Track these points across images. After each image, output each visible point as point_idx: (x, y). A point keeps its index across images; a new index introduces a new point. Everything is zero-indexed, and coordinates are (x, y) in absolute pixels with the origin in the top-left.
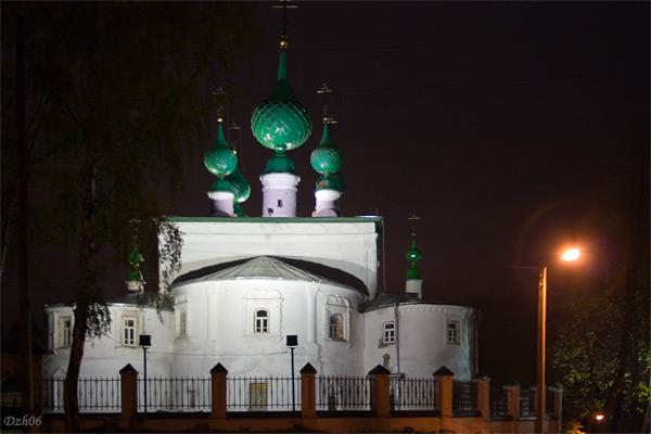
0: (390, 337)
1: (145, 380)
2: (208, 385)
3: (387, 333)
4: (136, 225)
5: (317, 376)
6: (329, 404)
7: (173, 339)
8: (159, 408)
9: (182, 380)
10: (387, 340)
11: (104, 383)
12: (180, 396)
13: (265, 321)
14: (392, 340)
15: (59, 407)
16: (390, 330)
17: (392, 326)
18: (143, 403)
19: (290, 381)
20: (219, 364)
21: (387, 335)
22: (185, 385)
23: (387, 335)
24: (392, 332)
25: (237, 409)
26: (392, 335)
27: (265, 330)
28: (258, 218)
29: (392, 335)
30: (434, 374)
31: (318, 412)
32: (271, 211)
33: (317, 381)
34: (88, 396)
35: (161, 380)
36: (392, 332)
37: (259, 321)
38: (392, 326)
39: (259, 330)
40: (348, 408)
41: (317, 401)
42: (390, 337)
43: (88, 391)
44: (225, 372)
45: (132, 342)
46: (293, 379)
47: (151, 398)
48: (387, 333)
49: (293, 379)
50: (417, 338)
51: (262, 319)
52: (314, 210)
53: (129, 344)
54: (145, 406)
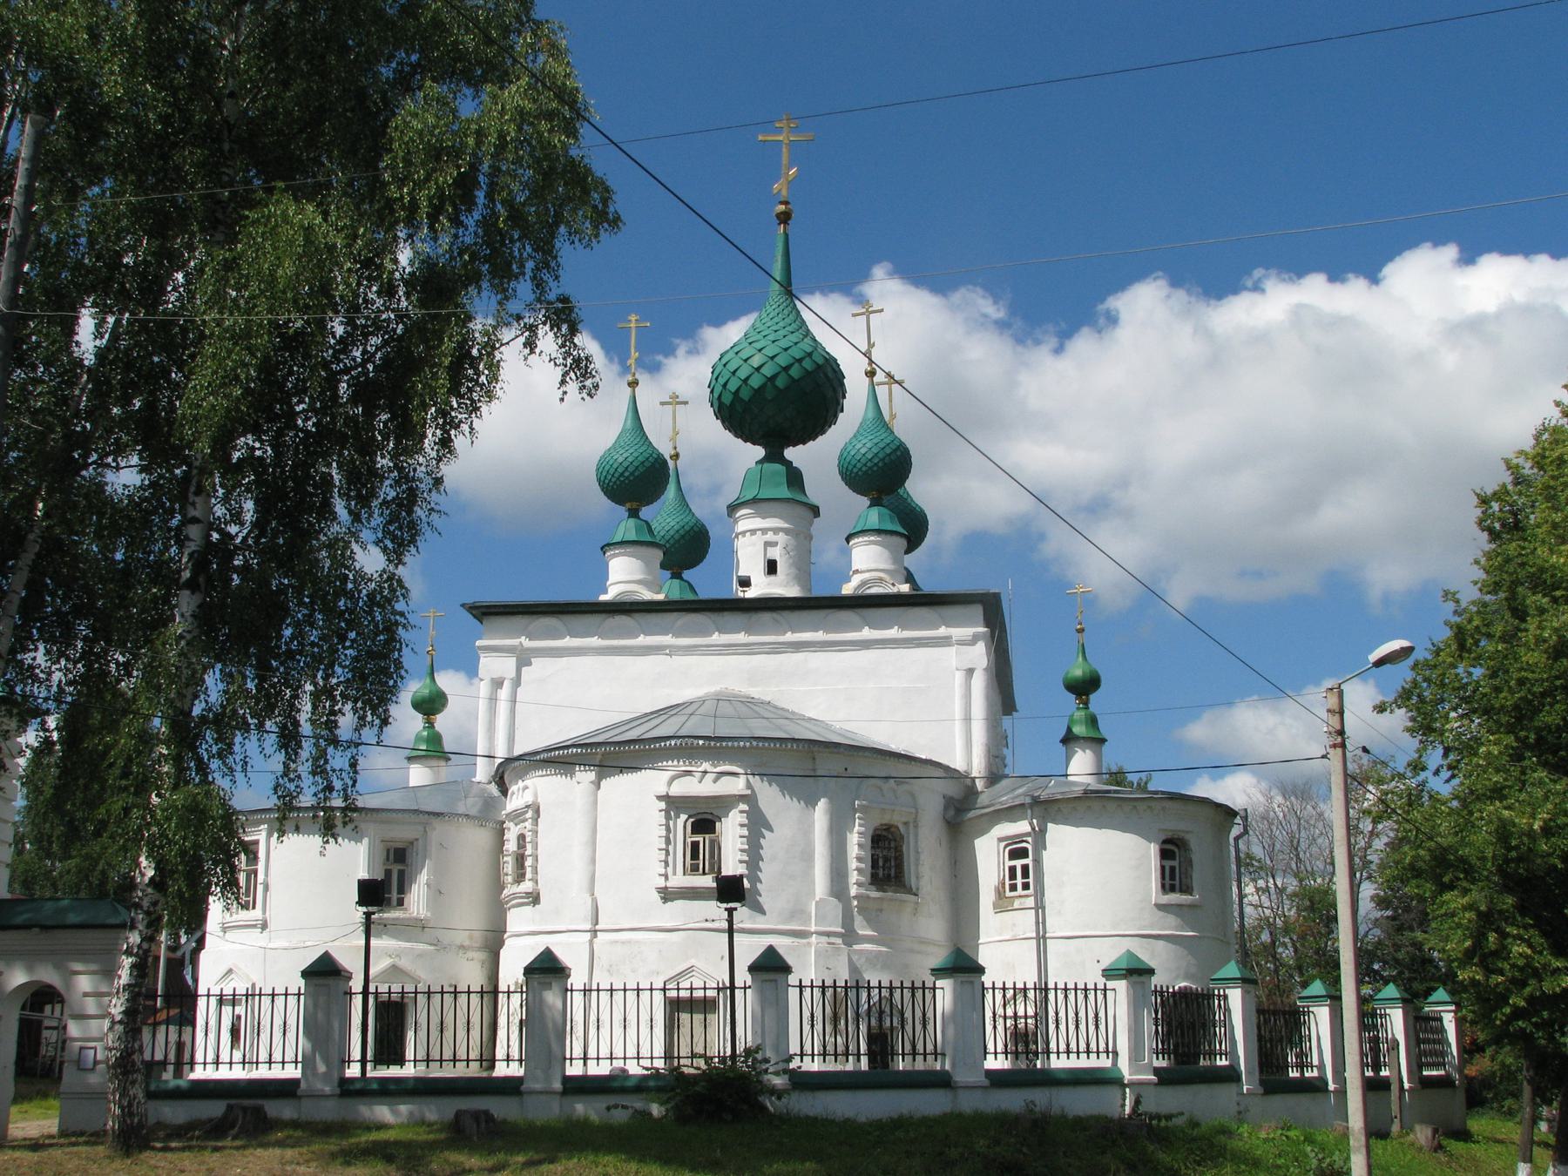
0: (1019, 881)
2: (294, 1012)
4: (18, 459)
5: (793, 979)
7: (1169, 835)
8: (618, 1064)
9: (429, 993)
12: (449, 1034)
14: (1026, 886)
16: (1018, 863)
17: (1022, 853)
18: (578, 1051)
21: (1013, 876)
22: (864, 995)
23: (1013, 876)
24: (1025, 868)
26: (1025, 874)
28: (999, 707)
29: (1025, 874)
31: (990, 1074)
32: (745, 583)
33: (793, 994)
35: (455, 993)
36: (1025, 868)
41: (850, 1067)
42: (1019, 881)
44: (786, 969)
45: (1026, 886)
46: (732, 987)
48: (1012, 870)
54: (585, 1059)
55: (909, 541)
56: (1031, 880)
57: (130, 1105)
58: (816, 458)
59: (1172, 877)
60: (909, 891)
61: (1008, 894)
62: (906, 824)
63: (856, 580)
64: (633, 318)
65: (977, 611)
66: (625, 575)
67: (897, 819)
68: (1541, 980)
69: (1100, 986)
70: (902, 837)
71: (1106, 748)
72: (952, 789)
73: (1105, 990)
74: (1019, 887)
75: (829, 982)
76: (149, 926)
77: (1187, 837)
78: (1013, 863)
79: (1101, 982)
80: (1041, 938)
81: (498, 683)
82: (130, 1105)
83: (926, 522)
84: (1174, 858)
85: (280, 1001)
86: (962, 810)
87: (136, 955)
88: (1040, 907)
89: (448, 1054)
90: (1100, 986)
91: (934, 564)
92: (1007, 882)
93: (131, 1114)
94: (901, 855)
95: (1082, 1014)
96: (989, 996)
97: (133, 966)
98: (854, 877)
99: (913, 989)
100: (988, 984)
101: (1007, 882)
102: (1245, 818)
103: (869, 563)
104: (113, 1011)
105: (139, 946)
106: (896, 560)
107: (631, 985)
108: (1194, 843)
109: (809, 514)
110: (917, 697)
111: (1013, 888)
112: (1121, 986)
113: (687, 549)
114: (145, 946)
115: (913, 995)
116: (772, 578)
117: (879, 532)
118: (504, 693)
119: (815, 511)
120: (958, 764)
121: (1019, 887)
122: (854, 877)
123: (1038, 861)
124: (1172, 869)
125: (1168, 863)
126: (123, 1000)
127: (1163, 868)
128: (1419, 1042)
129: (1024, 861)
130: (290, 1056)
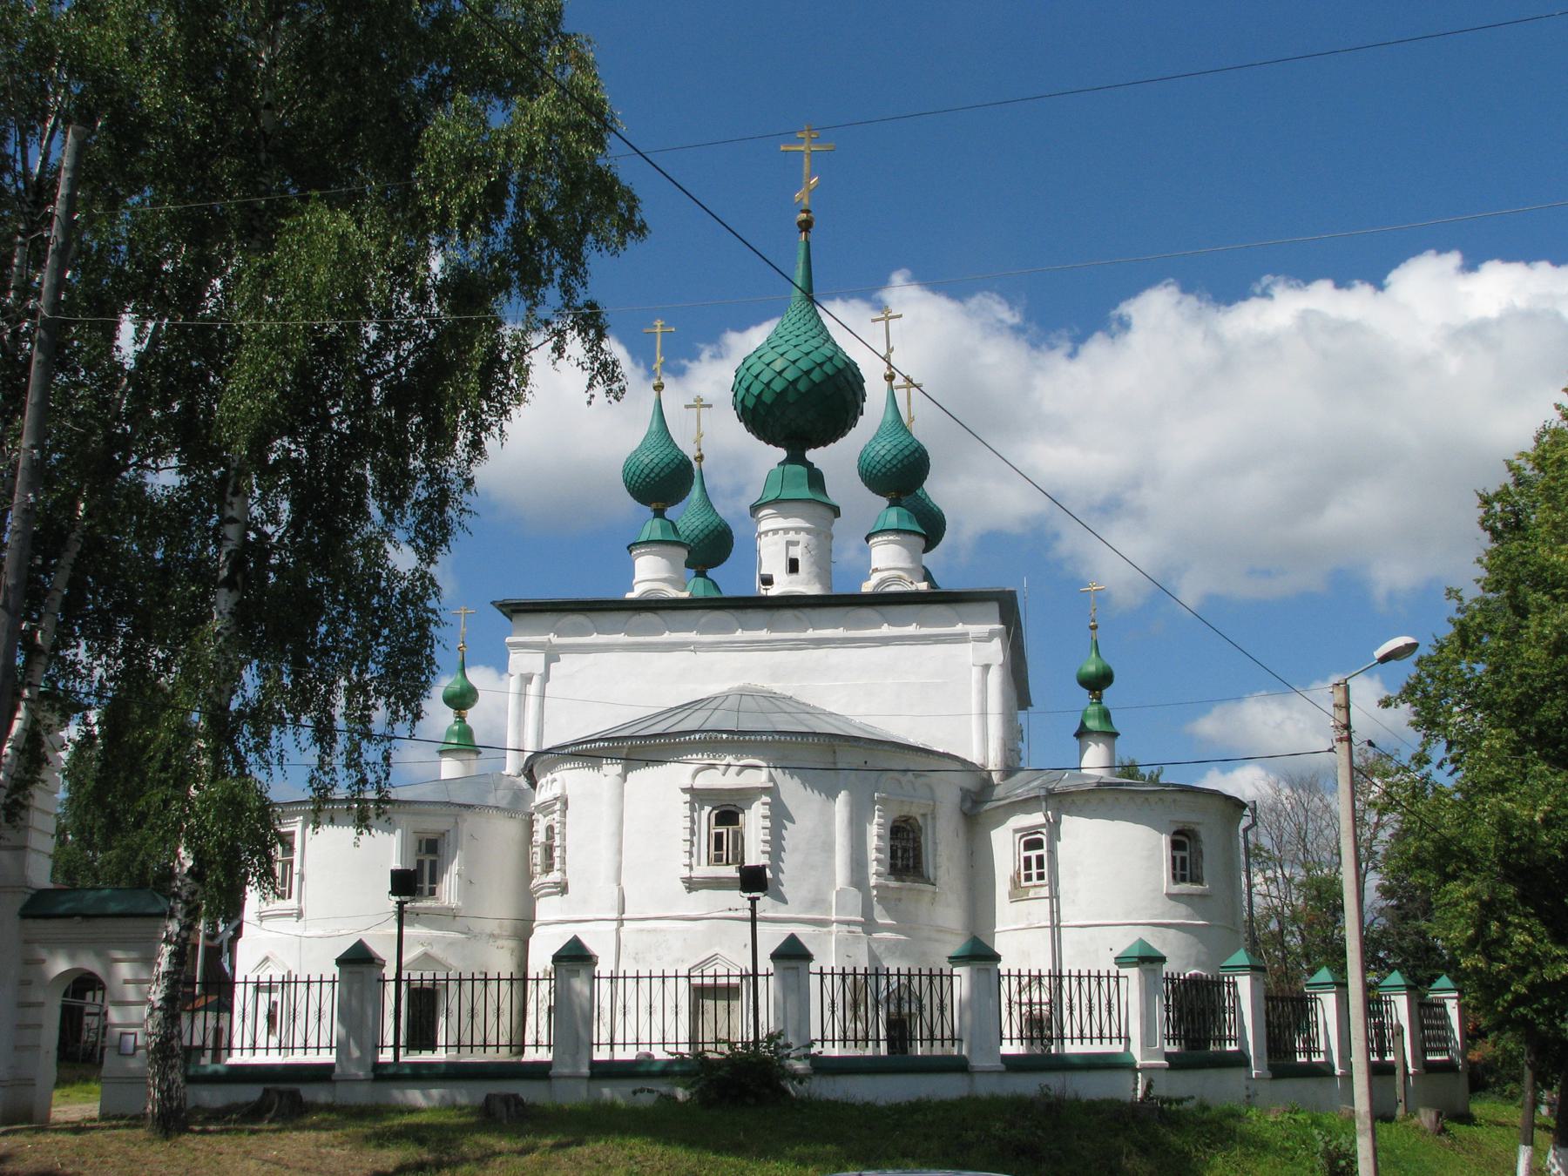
0: (1034, 871)
1: (398, 980)
2: (328, 998)
5: (814, 967)
6: (889, 1039)
7: (1180, 826)
8: (644, 1049)
9: (460, 980)
10: (1028, 878)
14: (1041, 876)
15: (537, 1045)
16: (1033, 854)
17: (1036, 844)
18: (605, 1037)
22: (883, 982)
24: (1040, 859)
33: (814, 981)
34: (491, 1019)
35: (486, 980)
36: (1040, 859)
40: (467, 1057)
42: (1034, 871)
45: (1041, 876)
46: (755, 975)
47: (628, 1029)
48: (1028, 860)
50: (43, 953)
54: (612, 1044)
57: (169, 1089)
58: (837, 460)
59: (1183, 868)
60: (927, 881)
61: (1023, 883)
62: (924, 815)
66: (650, 574)
67: (915, 811)
70: (920, 829)
71: (1118, 741)
72: (969, 782)
74: (1034, 877)
76: (188, 914)
77: (1198, 828)
78: (1028, 853)
79: (1114, 970)
80: (1056, 927)
81: (527, 679)
82: (169, 1089)
84: (1184, 849)
85: (315, 988)
86: (978, 803)
87: (175, 943)
88: (1054, 896)
89: (478, 1040)
91: (951, 562)
93: (170, 1098)
94: (920, 846)
95: (1095, 1001)
96: (1005, 983)
97: (172, 954)
98: (873, 867)
99: (931, 976)
100: (1004, 972)
101: (1023, 872)
102: (1254, 810)
103: (888, 562)
104: (153, 998)
105: (178, 935)
106: (915, 559)
107: (1035, 973)
108: (1204, 834)
110: (934, 692)
111: (1028, 878)
112: (1133, 973)
113: (711, 548)
114: (184, 934)
116: (794, 576)
117: (897, 531)
118: (533, 689)
119: (836, 511)
120: (975, 757)
121: (1034, 877)
122: (873, 867)
123: (1052, 852)
124: (1183, 860)
125: (1179, 854)
127: (1174, 858)
128: (1423, 1027)
130: (324, 1041)
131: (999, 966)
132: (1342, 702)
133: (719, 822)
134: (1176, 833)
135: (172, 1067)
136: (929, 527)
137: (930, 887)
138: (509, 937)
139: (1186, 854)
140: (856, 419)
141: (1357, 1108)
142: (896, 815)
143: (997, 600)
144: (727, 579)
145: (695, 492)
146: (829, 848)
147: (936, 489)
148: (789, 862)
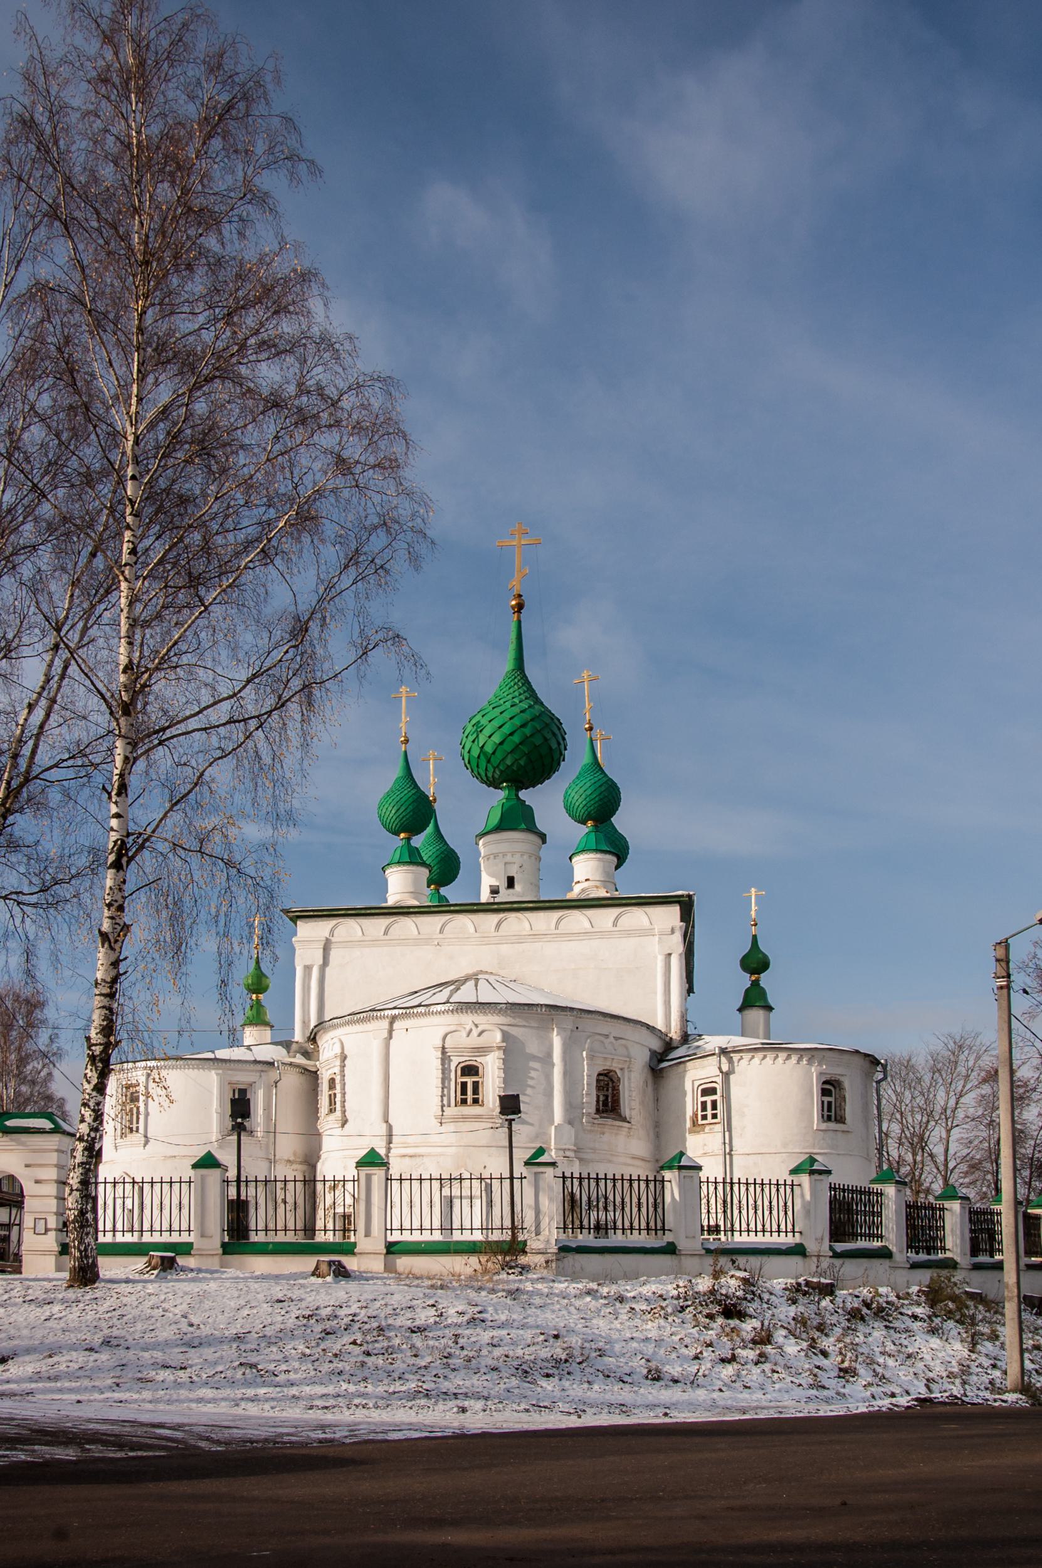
0: (709, 1112)
3: (704, 1104)
7: (828, 1077)
9: (115, 1183)
10: (704, 1117)
11: (166, 1187)
13: (476, 1086)
14: (714, 1116)
16: (709, 1099)
17: (713, 1091)
19: (507, 1183)
20: (373, 1149)
21: (704, 1108)
23: (704, 1108)
25: (467, 1236)
26: (714, 1107)
27: (476, 1101)
29: (714, 1107)
30: (195, 1166)
35: (115, 1183)
36: (714, 1104)
37: (464, 1085)
38: (713, 1091)
39: (464, 1102)
42: (709, 1112)
43: (735, 1201)
45: (714, 1116)
46: (512, 1178)
48: (704, 1104)
49: (512, 1178)
51: (469, 1080)
52: (296, 934)
53: (710, 1120)
55: (619, 858)
56: (718, 1112)
57: (86, 1250)
59: (829, 1110)
60: (624, 1120)
61: (700, 1122)
62: (622, 1069)
63: (577, 889)
64: (403, 689)
65: (676, 910)
66: (400, 884)
67: (615, 1066)
68: (843, 1329)
69: (789, 1182)
70: (619, 1080)
71: (772, 1014)
72: (656, 1045)
73: (792, 1185)
74: (709, 1117)
75: (585, 1175)
76: (95, 1120)
77: (842, 1079)
78: (704, 1099)
82: (86, 1250)
83: (628, 848)
84: (830, 1095)
87: (87, 1141)
90: (789, 1182)
92: (700, 1114)
93: (87, 1257)
94: (618, 1093)
95: (774, 1203)
96: (704, 1188)
97: (85, 1149)
100: (704, 1179)
101: (700, 1114)
102: (884, 1067)
104: (71, 1182)
105: (89, 1135)
106: (606, 873)
108: (846, 1084)
109: (539, 841)
111: (704, 1117)
112: (805, 1179)
113: (446, 868)
114: (93, 1134)
115: (647, 1186)
116: (511, 891)
119: (543, 837)
120: (660, 1025)
121: (709, 1117)
123: (727, 1098)
124: (829, 1103)
125: (826, 1099)
126: (78, 1174)
127: (823, 1102)
129: (713, 1097)
131: (701, 1174)
132: (1003, 957)
133: (463, 1074)
134: (825, 1083)
135: (87, 1234)
136: (617, 849)
137: (626, 1124)
138: (301, 1163)
139: (829, 1099)
140: (559, 764)
141: (1006, 1279)
142: (600, 1069)
143: (678, 902)
144: (453, 893)
145: (430, 829)
146: (549, 1094)
147: (620, 821)
148: (262, 1264)
